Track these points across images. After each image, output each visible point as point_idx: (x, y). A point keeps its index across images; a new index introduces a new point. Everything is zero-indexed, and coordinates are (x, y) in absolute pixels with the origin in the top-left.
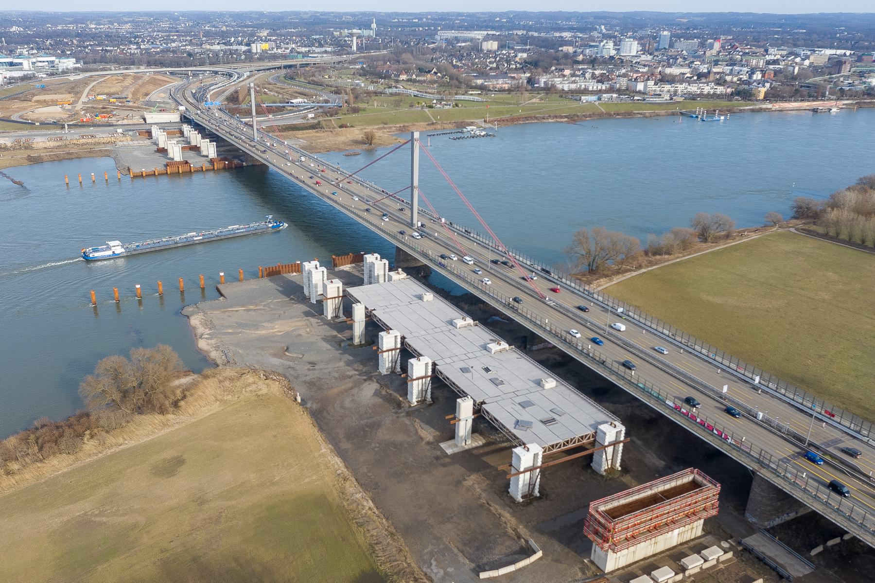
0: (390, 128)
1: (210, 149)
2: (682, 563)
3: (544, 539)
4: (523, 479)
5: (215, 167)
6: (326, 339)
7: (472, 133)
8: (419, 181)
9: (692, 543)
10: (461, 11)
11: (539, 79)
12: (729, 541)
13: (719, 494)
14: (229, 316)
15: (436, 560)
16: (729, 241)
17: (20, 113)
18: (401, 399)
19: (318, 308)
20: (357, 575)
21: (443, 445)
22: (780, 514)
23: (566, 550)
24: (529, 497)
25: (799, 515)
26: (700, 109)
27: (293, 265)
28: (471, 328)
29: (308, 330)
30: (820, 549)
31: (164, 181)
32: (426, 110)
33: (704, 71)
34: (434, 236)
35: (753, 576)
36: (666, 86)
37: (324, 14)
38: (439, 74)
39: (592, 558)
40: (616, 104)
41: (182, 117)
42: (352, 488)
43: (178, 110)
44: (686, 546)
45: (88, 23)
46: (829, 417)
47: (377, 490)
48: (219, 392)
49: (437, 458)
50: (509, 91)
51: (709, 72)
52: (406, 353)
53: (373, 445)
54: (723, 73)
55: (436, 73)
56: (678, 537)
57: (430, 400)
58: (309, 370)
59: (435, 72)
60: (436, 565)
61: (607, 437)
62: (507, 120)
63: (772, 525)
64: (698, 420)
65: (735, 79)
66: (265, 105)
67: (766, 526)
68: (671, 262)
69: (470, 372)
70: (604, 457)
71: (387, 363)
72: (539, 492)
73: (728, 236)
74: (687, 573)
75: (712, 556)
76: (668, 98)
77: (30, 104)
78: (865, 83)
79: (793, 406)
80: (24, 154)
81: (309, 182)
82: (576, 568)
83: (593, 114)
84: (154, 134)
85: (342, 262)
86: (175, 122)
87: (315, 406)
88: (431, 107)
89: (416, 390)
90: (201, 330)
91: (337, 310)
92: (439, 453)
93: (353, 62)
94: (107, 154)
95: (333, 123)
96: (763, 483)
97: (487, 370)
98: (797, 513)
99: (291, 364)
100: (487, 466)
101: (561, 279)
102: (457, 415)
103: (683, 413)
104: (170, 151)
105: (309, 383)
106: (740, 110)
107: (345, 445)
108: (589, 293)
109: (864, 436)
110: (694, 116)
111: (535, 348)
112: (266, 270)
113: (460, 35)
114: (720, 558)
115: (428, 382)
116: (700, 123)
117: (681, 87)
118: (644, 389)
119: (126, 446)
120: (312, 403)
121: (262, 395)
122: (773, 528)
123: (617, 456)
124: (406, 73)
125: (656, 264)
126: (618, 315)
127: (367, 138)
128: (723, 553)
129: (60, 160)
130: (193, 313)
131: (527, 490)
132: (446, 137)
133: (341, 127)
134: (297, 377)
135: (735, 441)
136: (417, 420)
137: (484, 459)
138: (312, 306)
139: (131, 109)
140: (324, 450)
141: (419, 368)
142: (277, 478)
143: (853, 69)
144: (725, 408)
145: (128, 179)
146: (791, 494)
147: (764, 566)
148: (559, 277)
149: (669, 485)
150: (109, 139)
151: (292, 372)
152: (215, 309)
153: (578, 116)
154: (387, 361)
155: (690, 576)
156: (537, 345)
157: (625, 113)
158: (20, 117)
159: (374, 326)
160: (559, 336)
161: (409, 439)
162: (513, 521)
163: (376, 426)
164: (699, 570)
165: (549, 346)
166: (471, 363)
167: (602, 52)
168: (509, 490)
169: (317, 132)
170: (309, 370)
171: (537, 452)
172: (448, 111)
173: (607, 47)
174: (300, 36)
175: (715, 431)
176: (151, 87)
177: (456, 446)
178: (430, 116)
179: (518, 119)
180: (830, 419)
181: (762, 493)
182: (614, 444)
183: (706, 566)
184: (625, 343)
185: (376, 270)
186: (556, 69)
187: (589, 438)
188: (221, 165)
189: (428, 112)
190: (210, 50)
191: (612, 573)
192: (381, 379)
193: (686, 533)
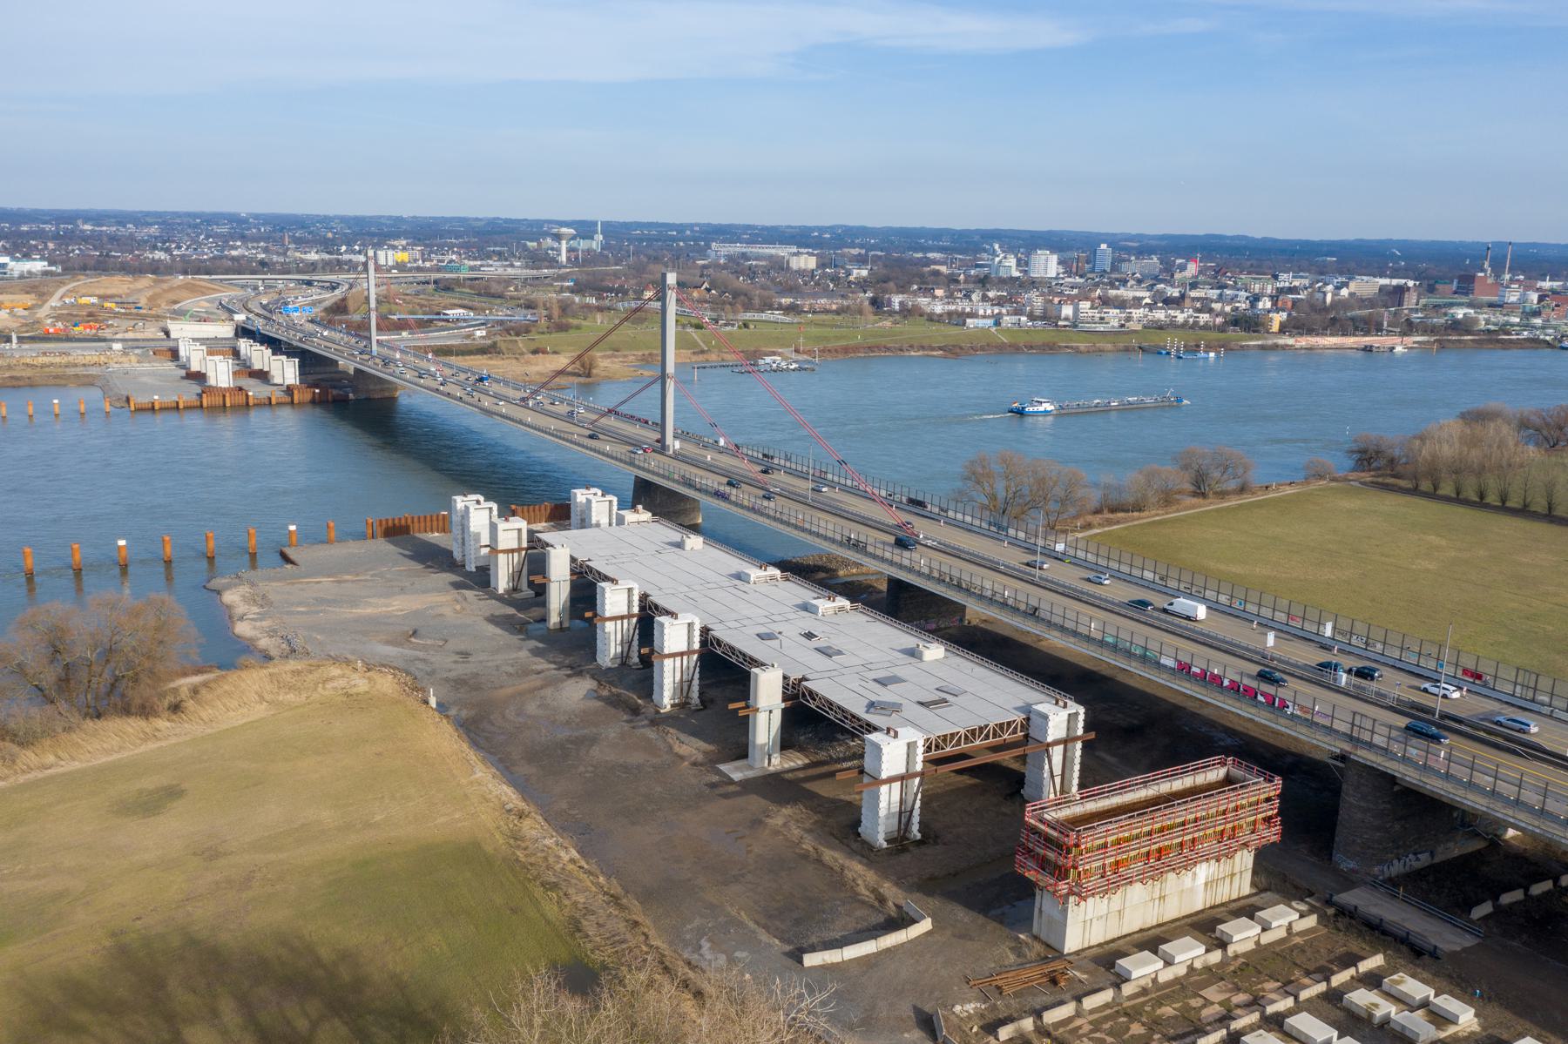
0: (625, 356)
1: (286, 371)
2: (1218, 934)
3: (934, 903)
4: (888, 799)
6: (493, 620)
7: (774, 365)
8: (676, 365)
9: (1234, 905)
11: (890, 299)
12: (1307, 899)
14: (302, 590)
15: (710, 940)
16: (1245, 496)
18: (640, 701)
19: (481, 578)
21: (724, 767)
23: (981, 919)
24: (899, 841)
25: (1437, 860)
26: (1172, 341)
27: (434, 518)
29: (458, 607)
31: (195, 421)
35: (1362, 953)
36: (1111, 311)
37: (507, 221)
38: (713, 292)
39: (1035, 930)
40: (1027, 332)
41: (240, 330)
42: (534, 827)
43: (233, 320)
44: (1223, 909)
45: (79, 222)
46: (1471, 680)
47: (587, 836)
48: (268, 687)
49: (713, 786)
50: (838, 312)
51: (1183, 296)
52: (647, 618)
53: (582, 769)
54: (1207, 299)
55: (708, 290)
56: (1206, 889)
57: (698, 701)
58: (455, 662)
59: (706, 289)
60: (710, 948)
61: (1050, 724)
62: (836, 351)
64: (1226, 683)
65: (1228, 309)
66: (395, 317)
67: (1376, 877)
68: (1145, 521)
69: (777, 638)
70: (1047, 767)
71: (613, 644)
72: (919, 831)
73: (1242, 490)
74: (1231, 950)
75: (1276, 919)
78: (1445, 314)
82: (1003, 947)
83: (988, 345)
84: (182, 353)
86: (225, 339)
87: (464, 714)
88: (698, 327)
89: (671, 677)
90: (241, 608)
91: (516, 576)
92: (715, 778)
93: (562, 278)
94: (87, 382)
95: (521, 345)
96: (1362, 781)
97: (810, 636)
98: (1432, 854)
99: (421, 654)
100: (813, 795)
101: (946, 511)
102: (751, 702)
103: (1195, 674)
104: (211, 374)
105: (455, 681)
106: (1242, 347)
107: (525, 769)
108: (999, 528)
109: (1543, 705)
110: (1164, 352)
112: (381, 525)
113: (750, 249)
114: (1294, 925)
115: (692, 664)
116: (1174, 361)
117: (1137, 313)
119: (60, 770)
120: (460, 710)
121: (357, 694)
123: (1072, 770)
130: (228, 587)
131: (896, 828)
132: (728, 371)
133: (535, 352)
134: (431, 673)
135: (1302, 708)
136: (671, 730)
137: (807, 786)
138: (469, 575)
139: (144, 318)
140: (479, 775)
141: (675, 637)
142: (378, 818)
143: (1423, 301)
146: (1421, 784)
147: (1382, 937)
148: (942, 510)
150: (96, 359)
151: (421, 665)
152: (270, 579)
153: (961, 348)
154: (613, 638)
155: (1236, 957)
157: (1044, 345)
159: (586, 586)
160: (948, 579)
161: (655, 761)
162: (871, 876)
163: (593, 740)
164: (1254, 947)
166: (775, 628)
167: (997, 271)
168: (860, 830)
169: (491, 358)
170: (455, 662)
171: (914, 740)
172: (730, 333)
173: (1007, 264)
174: (467, 248)
175: (1260, 698)
176: (184, 293)
177: (751, 767)
178: (699, 341)
179: (856, 349)
181: (1362, 804)
182: (1066, 742)
183: (1266, 939)
185: (593, 514)
186: (920, 289)
187: (1015, 732)
188: (308, 396)
189: (696, 337)
190: (302, 261)
191: (1077, 953)
192: (601, 675)
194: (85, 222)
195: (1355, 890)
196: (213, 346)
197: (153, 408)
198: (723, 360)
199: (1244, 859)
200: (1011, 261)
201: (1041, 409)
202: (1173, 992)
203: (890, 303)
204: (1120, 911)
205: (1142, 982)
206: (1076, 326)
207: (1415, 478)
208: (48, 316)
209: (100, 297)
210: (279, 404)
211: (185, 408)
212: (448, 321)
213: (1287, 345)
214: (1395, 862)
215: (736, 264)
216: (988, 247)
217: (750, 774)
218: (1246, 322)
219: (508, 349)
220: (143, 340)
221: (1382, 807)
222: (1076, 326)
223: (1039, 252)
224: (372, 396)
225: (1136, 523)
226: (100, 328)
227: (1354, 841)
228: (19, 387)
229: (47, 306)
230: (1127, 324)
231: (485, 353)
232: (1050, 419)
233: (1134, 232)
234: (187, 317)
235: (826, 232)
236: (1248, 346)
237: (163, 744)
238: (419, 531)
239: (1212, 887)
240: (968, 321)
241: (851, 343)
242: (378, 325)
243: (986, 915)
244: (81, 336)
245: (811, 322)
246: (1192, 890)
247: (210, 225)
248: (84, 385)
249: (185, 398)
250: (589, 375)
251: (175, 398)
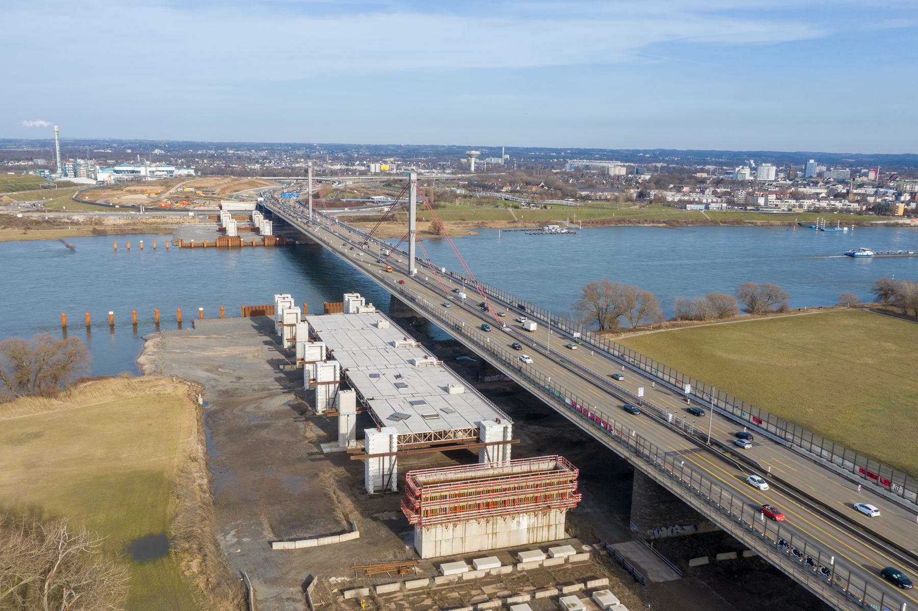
0: (467, 223)
1: (267, 228)
5: (266, 242)
7: (553, 230)
10: (602, 148)
11: (649, 193)
12: (595, 545)
13: (578, 479)
20: (142, 536)
21: (322, 445)
26: (822, 221)
28: (411, 349)
30: (704, 561)
31: (214, 252)
33: (842, 191)
34: (424, 281)
40: (724, 213)
45: (228, 149)
55: (543, 186)
58: (232, 382)
62: (597, 222)
63: (657, 536)
66: (344, 200)
73: (781, 310)
74: (520, 567)
76: (786, 209)
79: (723, 416)
83: (696, 221)
85: (334, 309)
94: (169, 232)
96: (639, 477)
98: (695, 527)
106: (872, 224)
112: (249, 310)
118: (549, 391)
124: (510, 185)
125: (678, 327)
128: (575, 552)
129: (124, 234)
144: (623, 404)
145: (177, 249)
149: (519, 467)
150: (178, 220)
153: (678, 222)
156: (490, 376)
157: (733, 221)
158: (106, 202)
167: (737, 177)
169: (389, 223)
173: (743, 172)
179: (609, 222)
186: (674, 187)
188: (273, 242)
189: (512, 212)
193: (540, 530)
194: (231, 149)
195: (629, 543)
196: (235, 215)
197: (191, 246)
198: (525, 227)
199: (558, 517)
202: (466, 585)
203: (649, 195)
204: (462, 538)
205: (451, 578)
206: (758, 210)
207: (904, 307)
208: (166, 198)
209: (196, 188)
210: (257, 246)
211: (207, 247)
212: (373, 202)
213: (905, 224)
214: (664, 529)
215: (579, 173)
216: (747, 162)
217: (335, 450)
218: (879, 209)
219: (401, 218)
220: (208, 211)
221: (650, 493)
222: (758, 210)
223: (763, 165)
224: (308, 243)
225: (695, 326)
227: (636, 513)
228: (135, 234)
229: (168, 192)
230: (793, 209)
231: (387, 220)
233: (854, 153)
234: (233, 198)
235: (648, 153)
236: (876, 224)
237: (51, 412)
238: (270, 314)
239: (533, 531)
240: (688, 206)
241: (609, 218)
242: (409, 210)
243: (396, 535)
244: (177, 208)
245: (592, 207)
246: (517, 531)
247: (294, 150)
249: (208, 241)
250: (438, 234)
251: (203, 241)
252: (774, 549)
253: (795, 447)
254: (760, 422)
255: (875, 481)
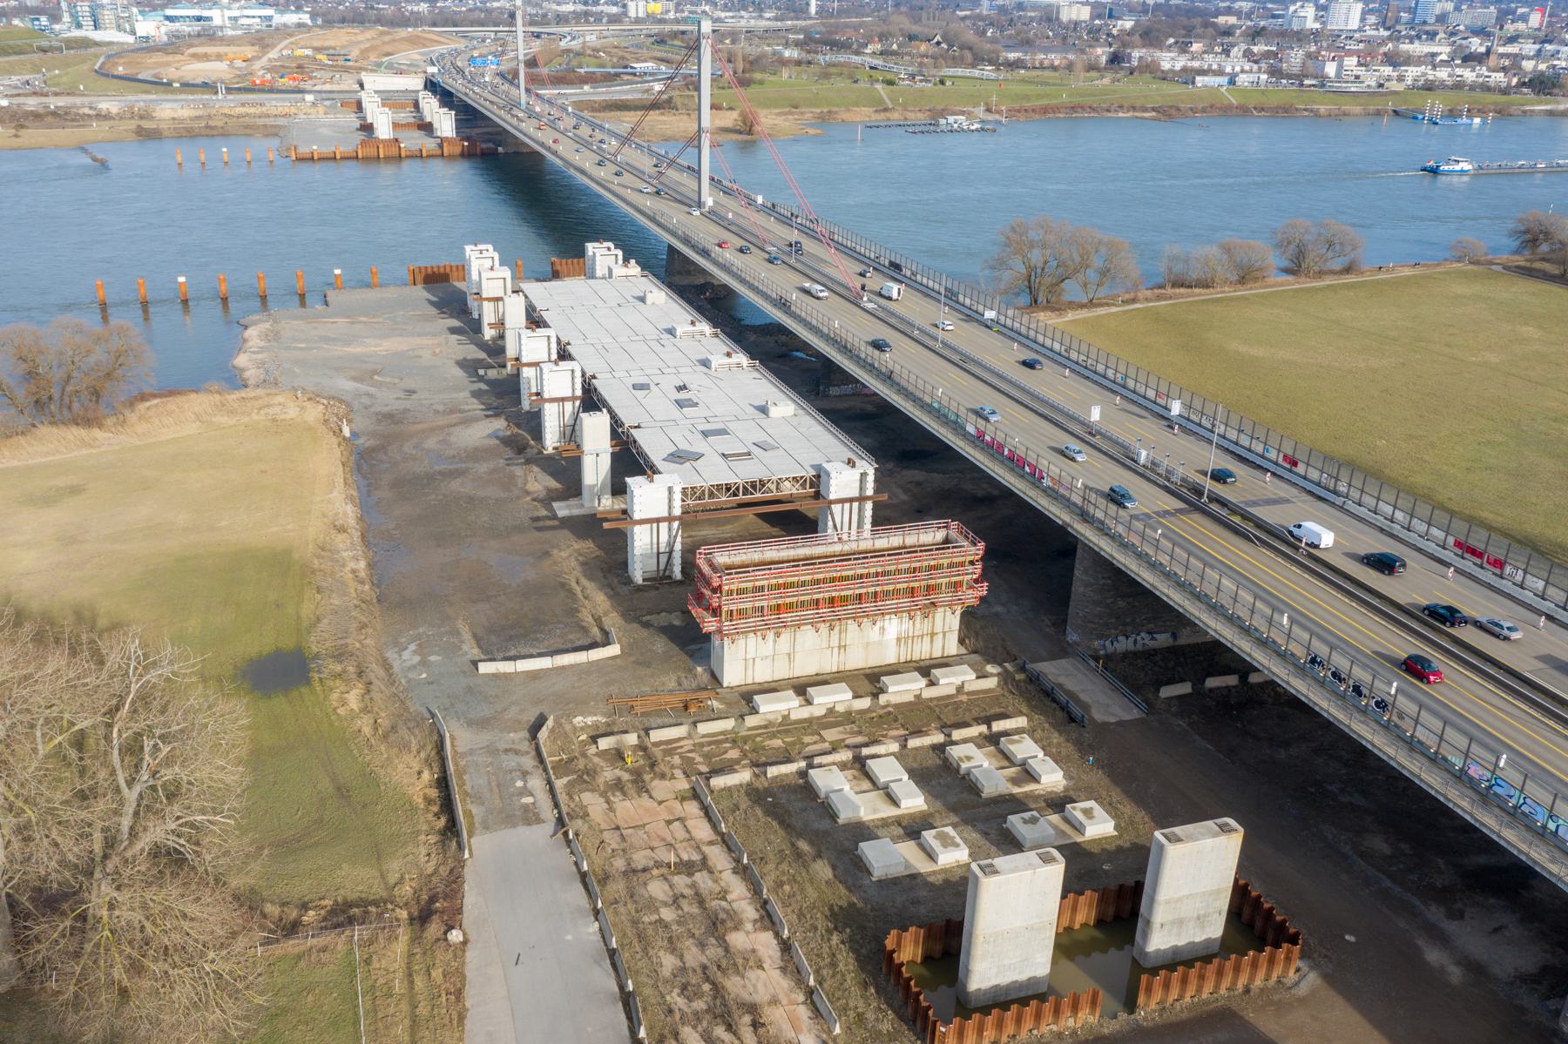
0: (802, 113)
13: (982, 559)
17: (154, 72)
21: (555, 505)
22: (1129, 628)
26: (1436, 105)
30: (1184, 688)
31: (352, 171)
32: (879, 86)
40: (1263, 92)
55: (938, 43)
63: (1110, 649)
66: (582, 71)
67: (1097, 651)
74: (883, 699)
77: (178, 57)
80: (133, 124)
81: (601, 173)
83: (1211, 107)
88: (890, 83)
94: (271, 132)
98: (1174, 636)
106: (1525, 112)
111: (834, 391)
122: (1108, 657)
124: (881, 40)
126: (987, 326)
127: (745, 123)
140: (335, 494)
142: (223, 523)
150: (287, 110)
153: (1178, 109)
157: (1277, 107)
158: (155, 76)
165: (866, 391)
167: (1290, 24)
169: (663, 114)
179: (1055, 109)
180: (1290, 471)
184: (966, 358)
186: (1176, 43)
188: (458, 150)
189: (882, 93)
195: (1063, 661)
198: (906, 119)
199: (947, 620)
200: (1310, 11)
201: (1458, 168)
205: (771, 717)
210: (430, 156)
211: (342, 158)
212: (635, 74)
217: (576, 512)
222: (1323, 86)
226: (303, 80)
229: (265, 59)
230: (1387, 84)
232: (1465, 179)
237: (94, 451)
240: (1198, 79)
245: (1024, 81)
246: (880, 643)
248: (267, 136)
249: (342, 149)
250: (750, 132)
251: (333, 149)
252: (1300, 670)
253: (1350, 506)
254: (1295, 464)
255: (1478, 561)
